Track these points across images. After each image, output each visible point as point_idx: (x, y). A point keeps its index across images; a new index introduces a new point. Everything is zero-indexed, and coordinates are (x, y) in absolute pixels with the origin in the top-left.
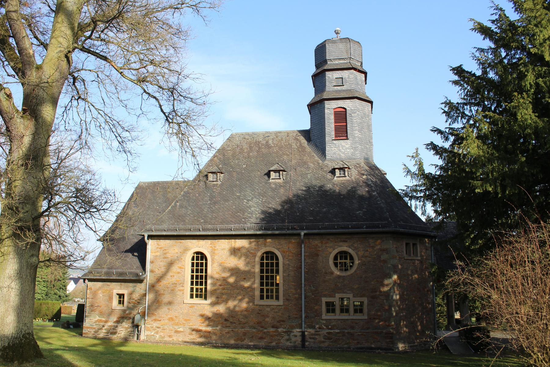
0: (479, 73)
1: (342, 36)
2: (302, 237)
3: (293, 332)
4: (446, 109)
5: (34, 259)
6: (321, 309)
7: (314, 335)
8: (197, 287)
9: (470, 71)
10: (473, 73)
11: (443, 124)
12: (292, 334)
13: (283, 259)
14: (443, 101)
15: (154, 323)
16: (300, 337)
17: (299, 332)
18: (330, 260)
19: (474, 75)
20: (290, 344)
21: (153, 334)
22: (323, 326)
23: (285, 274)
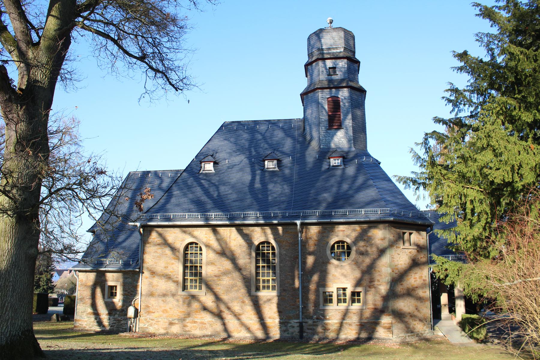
0: (487, 59)
1: (334, 25)
2: (299, 227)
3: (291, 323)
4: (453, 98)
5: (32, 251)
6: (319, 299)
7: (312, 325)
8: (264, 278)
9: (477, 57)
10: (480, 59)
11: (447, 112)
12: (289, 325)
13: (280, 249)
14: (449, 87)
15: (148, 315)
16: (298, 328)
17: (296, 323)
18: (327, 250)
19: (481, 61)
20: (287, 335)
21: (146, 326)
22: (321, 317)
23: (281, 265)
